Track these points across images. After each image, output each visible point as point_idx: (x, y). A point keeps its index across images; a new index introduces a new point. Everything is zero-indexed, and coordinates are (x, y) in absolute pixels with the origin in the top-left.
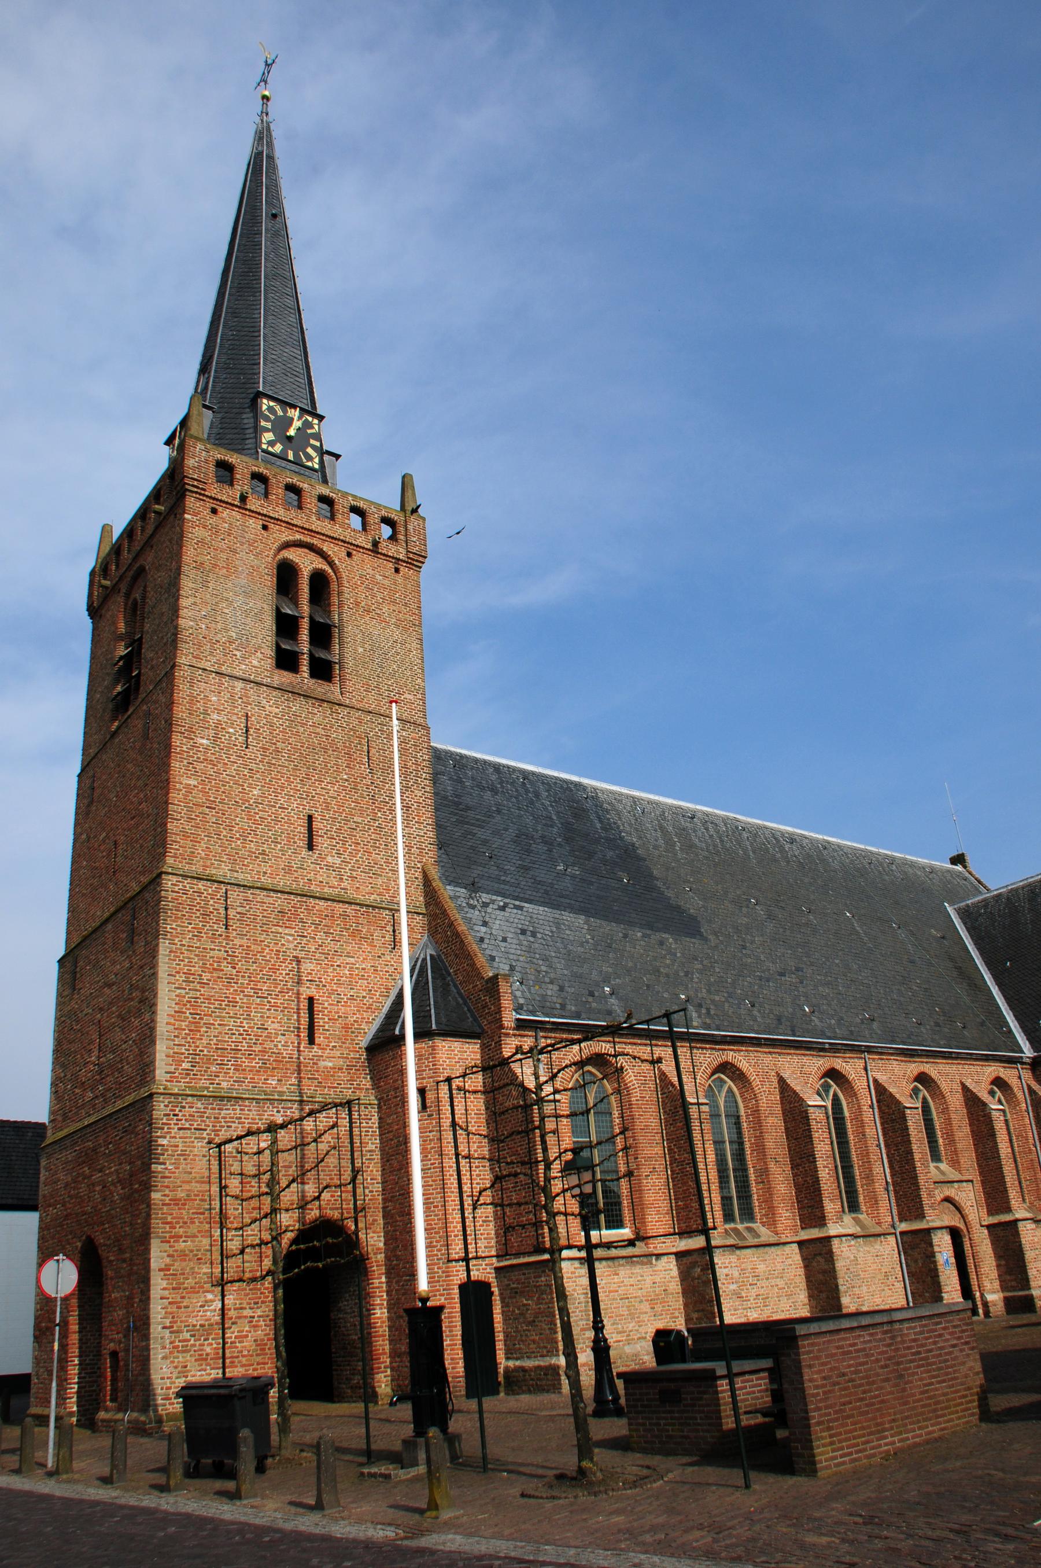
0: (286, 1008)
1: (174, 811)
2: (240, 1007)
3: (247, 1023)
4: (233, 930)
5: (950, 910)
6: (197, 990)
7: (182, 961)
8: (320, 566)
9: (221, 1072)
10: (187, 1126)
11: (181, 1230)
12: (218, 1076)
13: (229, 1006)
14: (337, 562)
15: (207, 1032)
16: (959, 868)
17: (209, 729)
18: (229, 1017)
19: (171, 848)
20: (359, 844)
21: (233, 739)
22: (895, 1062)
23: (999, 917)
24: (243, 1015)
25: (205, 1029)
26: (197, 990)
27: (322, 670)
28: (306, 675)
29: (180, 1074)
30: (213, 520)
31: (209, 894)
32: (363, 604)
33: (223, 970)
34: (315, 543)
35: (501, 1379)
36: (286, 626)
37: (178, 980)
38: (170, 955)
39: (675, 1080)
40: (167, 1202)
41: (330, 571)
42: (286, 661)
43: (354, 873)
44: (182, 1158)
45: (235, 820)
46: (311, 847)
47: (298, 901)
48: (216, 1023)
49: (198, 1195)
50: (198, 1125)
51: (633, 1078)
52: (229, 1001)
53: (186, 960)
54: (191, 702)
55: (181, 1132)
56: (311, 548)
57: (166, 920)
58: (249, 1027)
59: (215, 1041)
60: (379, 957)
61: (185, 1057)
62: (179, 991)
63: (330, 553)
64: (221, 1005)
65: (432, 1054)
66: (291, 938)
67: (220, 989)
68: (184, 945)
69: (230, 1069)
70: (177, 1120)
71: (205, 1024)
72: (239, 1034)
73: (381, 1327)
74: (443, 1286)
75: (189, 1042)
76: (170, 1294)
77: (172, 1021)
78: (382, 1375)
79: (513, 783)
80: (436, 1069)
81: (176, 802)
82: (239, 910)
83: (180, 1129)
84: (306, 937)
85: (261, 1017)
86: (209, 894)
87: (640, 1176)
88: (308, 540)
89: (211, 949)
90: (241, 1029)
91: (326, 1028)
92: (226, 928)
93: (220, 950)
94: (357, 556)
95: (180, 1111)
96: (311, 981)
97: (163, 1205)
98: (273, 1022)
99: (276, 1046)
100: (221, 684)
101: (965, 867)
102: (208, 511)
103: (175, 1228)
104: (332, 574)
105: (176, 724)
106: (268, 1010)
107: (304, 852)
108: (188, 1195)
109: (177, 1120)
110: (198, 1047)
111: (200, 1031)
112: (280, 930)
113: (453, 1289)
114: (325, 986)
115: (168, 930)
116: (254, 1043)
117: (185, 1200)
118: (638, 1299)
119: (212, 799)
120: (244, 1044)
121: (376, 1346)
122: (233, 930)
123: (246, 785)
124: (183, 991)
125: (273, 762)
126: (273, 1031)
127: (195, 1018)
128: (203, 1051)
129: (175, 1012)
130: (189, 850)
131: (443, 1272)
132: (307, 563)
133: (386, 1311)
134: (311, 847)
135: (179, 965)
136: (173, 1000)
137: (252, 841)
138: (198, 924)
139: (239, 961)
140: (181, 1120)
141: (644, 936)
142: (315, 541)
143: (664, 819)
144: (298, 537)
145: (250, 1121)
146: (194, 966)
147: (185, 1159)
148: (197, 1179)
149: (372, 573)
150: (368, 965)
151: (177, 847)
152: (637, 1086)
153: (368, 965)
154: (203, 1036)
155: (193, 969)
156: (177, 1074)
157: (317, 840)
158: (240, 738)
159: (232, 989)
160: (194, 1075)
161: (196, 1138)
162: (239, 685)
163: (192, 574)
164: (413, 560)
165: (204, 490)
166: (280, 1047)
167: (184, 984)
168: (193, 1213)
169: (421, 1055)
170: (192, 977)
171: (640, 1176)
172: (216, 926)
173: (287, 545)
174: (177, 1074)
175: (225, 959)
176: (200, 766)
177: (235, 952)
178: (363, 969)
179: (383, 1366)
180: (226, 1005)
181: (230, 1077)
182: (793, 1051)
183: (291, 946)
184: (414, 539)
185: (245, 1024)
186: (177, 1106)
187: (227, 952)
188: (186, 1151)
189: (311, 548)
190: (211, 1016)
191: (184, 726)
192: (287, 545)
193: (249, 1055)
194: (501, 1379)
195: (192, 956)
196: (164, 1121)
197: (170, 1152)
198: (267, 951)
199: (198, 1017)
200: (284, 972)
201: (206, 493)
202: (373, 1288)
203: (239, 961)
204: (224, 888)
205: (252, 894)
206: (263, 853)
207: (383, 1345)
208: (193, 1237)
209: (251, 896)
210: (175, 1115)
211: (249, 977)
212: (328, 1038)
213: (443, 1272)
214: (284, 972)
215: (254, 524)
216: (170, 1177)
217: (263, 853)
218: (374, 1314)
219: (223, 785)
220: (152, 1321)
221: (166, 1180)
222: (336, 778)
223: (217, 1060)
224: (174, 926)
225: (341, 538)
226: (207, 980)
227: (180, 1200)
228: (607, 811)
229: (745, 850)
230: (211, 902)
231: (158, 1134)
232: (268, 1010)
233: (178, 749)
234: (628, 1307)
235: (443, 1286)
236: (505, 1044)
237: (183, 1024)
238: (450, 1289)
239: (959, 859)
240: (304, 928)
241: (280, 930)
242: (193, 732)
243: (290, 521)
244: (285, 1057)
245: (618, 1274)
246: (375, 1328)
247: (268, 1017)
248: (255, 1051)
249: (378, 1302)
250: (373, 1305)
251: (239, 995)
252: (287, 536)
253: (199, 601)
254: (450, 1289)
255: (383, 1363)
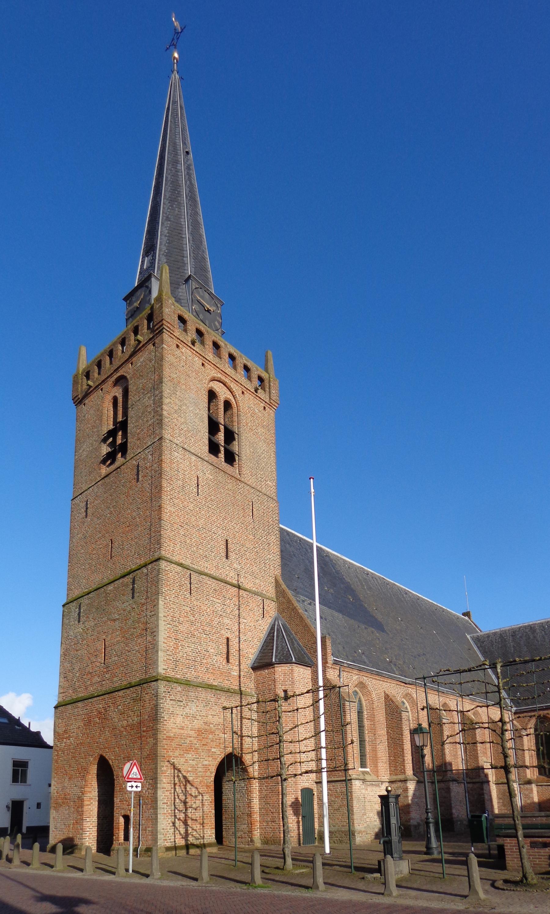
0: (217, 642)
1: (164, 525)
2: (197, 638)
3: (200, 647)
4: (193, 596)
5: (468, 637)
6: (177, 627)
7: (170, 609)
8: (228, 396)
9: (188, 672)
10: (174, 699)
11: (171, 753)
12: (187, 674)
13: (192, 637)
14: (237, 396)
15: (182, 650)
16: (466, 618)
17: (179, 480)
18: (192, 643)
19: (163, 546)
20: (248, 559)
21: (191, 489)
22: (467, 704)
23: (496, 643)
24: (198, 643)
25: (181, 648)
26: (177, 627)
27: (230, 458)
28: (223, 460)
29: (170, 670)
30: (178, 352)
31: (182, 575)
32: (249, 424)
33: (189, 617)
34: (227, 381)
35: (316, 836)
36: (213, 426)
37: (168, 620)
38: (164, 606)
39: (415, 698)
40: (165, 738)
41: (233, 401)
42: (214, 449)
43: (246, 575)
44: (172, 715)
45: (193, 536)
46: (227, 557)
47: (222, 586)
48: (186, 645)
49: (179, 736)
50: (179, 698)
51: (375, 696)
52: (191, 635)
53: (172, 609)
54: (170, 462)
55: (171, 702)
56: (224, 384)
57: (162, 586)
58: (200, 650)
59: (185, 655)
60: (257, 621)
61: (172, 662)
62: (169, 626)
63: (234, 389)
64: (188, 636)
65: (291, 673)
66: (219, 605)
67: (188, 627)
68: (171, 601)
69: (192, 671)
70: (170, 695)
71: (181, 645)
72: (197, 653)
73: (256, 808)
74: (293, 789)
75: (174, 654)
76: (166, 786)
77: (166, 641)
78: (256, 832)
79: (296, 542)
80: (293, 681)
81: (165, 520)
82: (196, 585)
83: (171, 700)
84: (226, 605)
85: (206, 645)
86: (182, 575)
87: (376, 743)
88: (223, 378)
89: (183, 605)
90: (197, 650)
91: (234, 655)
92: (190, 595)
93: (187, 606)
94: (247, 395)
95: (171, 690)
96: (228, 629)
97: (163, 739)
98: (211, 648)
99: (213, 661)
100: (185, 456)
101: (470, 618)
102: (175, 345)
103: (169, 752)
104: (235, 403)
105: (164, 474)
106: (209, 641)
107: (224, 559)
108: (174, 735)
109: (170, 695)
110: (178, 657)
111: (178, 649)
112: (214, 600)
113: (298, 791)
114: (234, 633)
115: (164, 591)
116: (203, 659)
117: (173, 737)
118: (374, 803)
119: (182, 521)
120: (198, 658)
121: (253, 817)
122: (193, 596)
123: (198, 517)
124: (171, 626)
125: (210, 506)
126: (211, 653)
127: (177, 642)
128: (180, 660)
129: (167, 637)
130: (172, 548)
131: (294, 783)
132: (223, 394)
133: (258, 800)
134: (227, 557)
135: (169, 611)
136: (166, 630)
137: (201, 549)
138: (177, 590)
139: (196, 613)
140: (171, 695)
141: (366, 628)
142: (227, 380)
143: (357, 573)
144: (219, 375)
145: (202, 699)
146: (175, 613)
147: (173, 716)
148: (179, 727)
149: (253, 407)
150: (252, 624)
151: (166, 545)
152: (376, 700)
153: (252, 624)
154: (180, 651)
155: (175, 614)
156: (168, 671)
157: (230, 554)
158: (194, 489)
159: (193, 628)
160: (176, 672)
161: (178, 706)
162: (194, 458)
163: (169, 384)
164: (273, 404)
165: (173, 331)
166: (214, 662)
167: (171, 622)
168: (177, 745)
169: (286, 673)
170: (175, 619)
171: (376, 743)
172: (185, 593)
173: (213, 379)
174: (168, 671)
175: (190, 611)
176: (176, 501)
177: (194, 609)
178: (250, 626)
179: (256, 827)
180: (190, 636)
181: (192, 675)
182: (432, 692)
183: (219, 609)
184: (274, 392)
185: (199, 648)
186: (170, 688)
187: (191, 608)
188: (174, 712)
189: (224, 384)
190: (183, 641)
191: (168, 476)
192: (213, 379)
193: (201, 664)
194: (316, 836)
195: (175, 608)
196: (164, 695)
197: (166, 712)
198: (208, 610)
199: (178, 641)
200: (216, 623)
201: (174, 334)
202: (253, 789)
203: (196, 613)
204: (189, 573)
205: (202, 578)
206: (206, 556)
207: (256, 817)
208: (176, 757)
209: (201, 579)
210: (168, 692)
211: (201, 623)
212: (235, 660)
213: (294, 783)
214: (216, 623)
215: (198, 361)
216: (166, 725)
217: (206, 556)
218: (253, 802)
219: (187, 515)
220: (158, 799)
221: (165, 726)
222: (238, 521)
223: (186, 665)
224: (166, 590)
225: (240, 382)
226: (182, 621)
227: (170, 737)
228: (335, 564)
229: (390, 594)
230: (183, 579)
231: (161, 702)
232: (209, 641)
233: (166, 489)
234: (371, 806)
235: (293, 789)
236: (328, 672)
237: (171, 644)
238: (297, 791)
239: (467, 614)
240: (224, 601)
241: (214, 600)
242: (172, 481)
243: (215, 364)
244: (216, 668)
245: (367, 790)
246: (253, 808)
247: (209, 646)
248: (203, 663)
249: (255, 796)
250: (253, 797)
251: (196, 632)
252: (215, 373)
253: (172, 402)
254: (297, 791)
255: (256, 826)
